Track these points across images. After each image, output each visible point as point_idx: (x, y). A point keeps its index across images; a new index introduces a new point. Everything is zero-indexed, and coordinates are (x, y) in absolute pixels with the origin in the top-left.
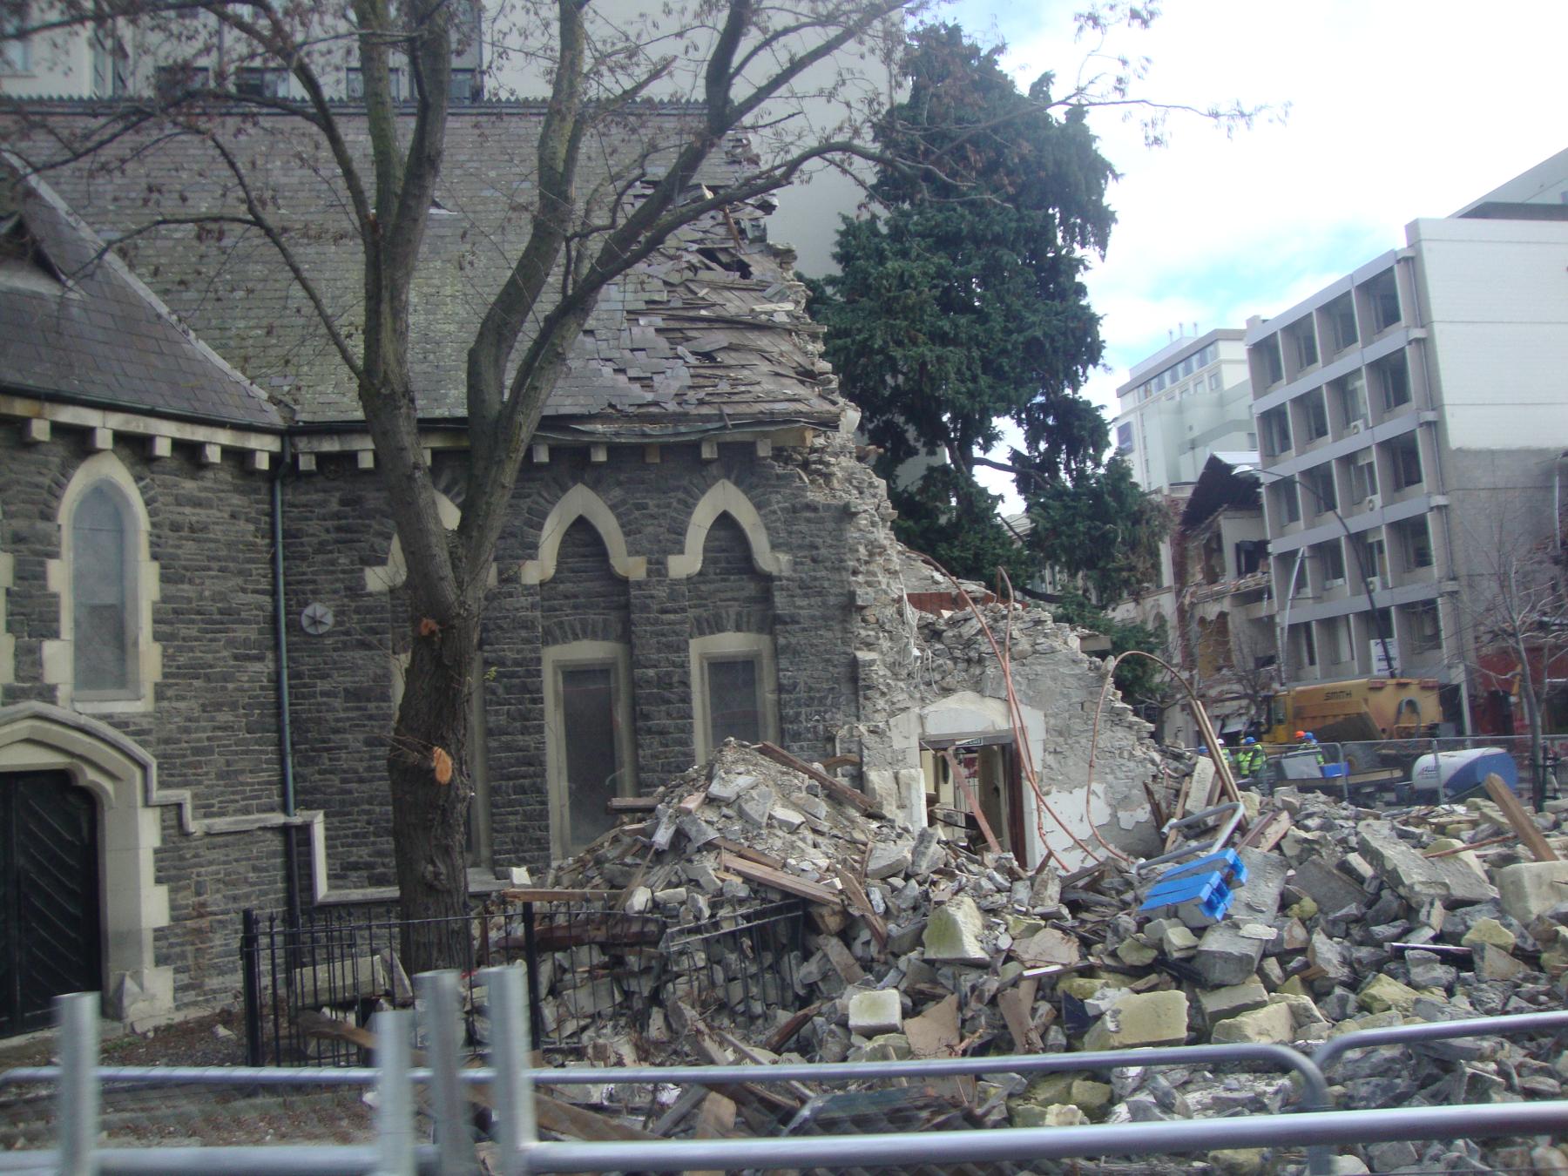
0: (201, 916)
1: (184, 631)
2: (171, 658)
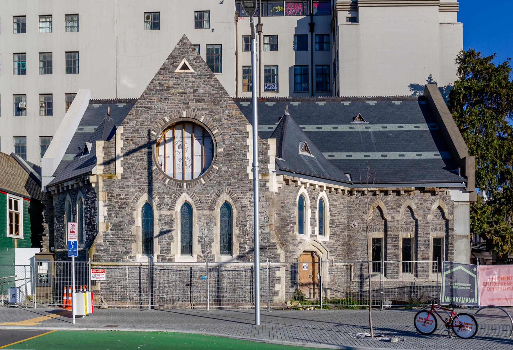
0: (334, 281)
1: (334, 226)
2: (331, 231)
